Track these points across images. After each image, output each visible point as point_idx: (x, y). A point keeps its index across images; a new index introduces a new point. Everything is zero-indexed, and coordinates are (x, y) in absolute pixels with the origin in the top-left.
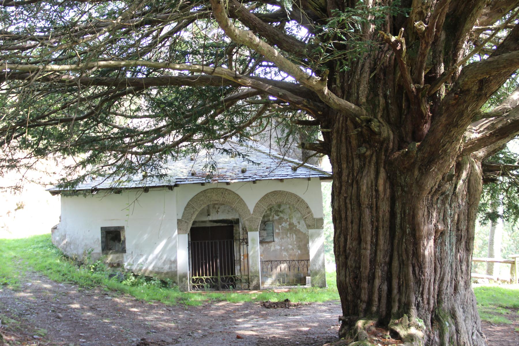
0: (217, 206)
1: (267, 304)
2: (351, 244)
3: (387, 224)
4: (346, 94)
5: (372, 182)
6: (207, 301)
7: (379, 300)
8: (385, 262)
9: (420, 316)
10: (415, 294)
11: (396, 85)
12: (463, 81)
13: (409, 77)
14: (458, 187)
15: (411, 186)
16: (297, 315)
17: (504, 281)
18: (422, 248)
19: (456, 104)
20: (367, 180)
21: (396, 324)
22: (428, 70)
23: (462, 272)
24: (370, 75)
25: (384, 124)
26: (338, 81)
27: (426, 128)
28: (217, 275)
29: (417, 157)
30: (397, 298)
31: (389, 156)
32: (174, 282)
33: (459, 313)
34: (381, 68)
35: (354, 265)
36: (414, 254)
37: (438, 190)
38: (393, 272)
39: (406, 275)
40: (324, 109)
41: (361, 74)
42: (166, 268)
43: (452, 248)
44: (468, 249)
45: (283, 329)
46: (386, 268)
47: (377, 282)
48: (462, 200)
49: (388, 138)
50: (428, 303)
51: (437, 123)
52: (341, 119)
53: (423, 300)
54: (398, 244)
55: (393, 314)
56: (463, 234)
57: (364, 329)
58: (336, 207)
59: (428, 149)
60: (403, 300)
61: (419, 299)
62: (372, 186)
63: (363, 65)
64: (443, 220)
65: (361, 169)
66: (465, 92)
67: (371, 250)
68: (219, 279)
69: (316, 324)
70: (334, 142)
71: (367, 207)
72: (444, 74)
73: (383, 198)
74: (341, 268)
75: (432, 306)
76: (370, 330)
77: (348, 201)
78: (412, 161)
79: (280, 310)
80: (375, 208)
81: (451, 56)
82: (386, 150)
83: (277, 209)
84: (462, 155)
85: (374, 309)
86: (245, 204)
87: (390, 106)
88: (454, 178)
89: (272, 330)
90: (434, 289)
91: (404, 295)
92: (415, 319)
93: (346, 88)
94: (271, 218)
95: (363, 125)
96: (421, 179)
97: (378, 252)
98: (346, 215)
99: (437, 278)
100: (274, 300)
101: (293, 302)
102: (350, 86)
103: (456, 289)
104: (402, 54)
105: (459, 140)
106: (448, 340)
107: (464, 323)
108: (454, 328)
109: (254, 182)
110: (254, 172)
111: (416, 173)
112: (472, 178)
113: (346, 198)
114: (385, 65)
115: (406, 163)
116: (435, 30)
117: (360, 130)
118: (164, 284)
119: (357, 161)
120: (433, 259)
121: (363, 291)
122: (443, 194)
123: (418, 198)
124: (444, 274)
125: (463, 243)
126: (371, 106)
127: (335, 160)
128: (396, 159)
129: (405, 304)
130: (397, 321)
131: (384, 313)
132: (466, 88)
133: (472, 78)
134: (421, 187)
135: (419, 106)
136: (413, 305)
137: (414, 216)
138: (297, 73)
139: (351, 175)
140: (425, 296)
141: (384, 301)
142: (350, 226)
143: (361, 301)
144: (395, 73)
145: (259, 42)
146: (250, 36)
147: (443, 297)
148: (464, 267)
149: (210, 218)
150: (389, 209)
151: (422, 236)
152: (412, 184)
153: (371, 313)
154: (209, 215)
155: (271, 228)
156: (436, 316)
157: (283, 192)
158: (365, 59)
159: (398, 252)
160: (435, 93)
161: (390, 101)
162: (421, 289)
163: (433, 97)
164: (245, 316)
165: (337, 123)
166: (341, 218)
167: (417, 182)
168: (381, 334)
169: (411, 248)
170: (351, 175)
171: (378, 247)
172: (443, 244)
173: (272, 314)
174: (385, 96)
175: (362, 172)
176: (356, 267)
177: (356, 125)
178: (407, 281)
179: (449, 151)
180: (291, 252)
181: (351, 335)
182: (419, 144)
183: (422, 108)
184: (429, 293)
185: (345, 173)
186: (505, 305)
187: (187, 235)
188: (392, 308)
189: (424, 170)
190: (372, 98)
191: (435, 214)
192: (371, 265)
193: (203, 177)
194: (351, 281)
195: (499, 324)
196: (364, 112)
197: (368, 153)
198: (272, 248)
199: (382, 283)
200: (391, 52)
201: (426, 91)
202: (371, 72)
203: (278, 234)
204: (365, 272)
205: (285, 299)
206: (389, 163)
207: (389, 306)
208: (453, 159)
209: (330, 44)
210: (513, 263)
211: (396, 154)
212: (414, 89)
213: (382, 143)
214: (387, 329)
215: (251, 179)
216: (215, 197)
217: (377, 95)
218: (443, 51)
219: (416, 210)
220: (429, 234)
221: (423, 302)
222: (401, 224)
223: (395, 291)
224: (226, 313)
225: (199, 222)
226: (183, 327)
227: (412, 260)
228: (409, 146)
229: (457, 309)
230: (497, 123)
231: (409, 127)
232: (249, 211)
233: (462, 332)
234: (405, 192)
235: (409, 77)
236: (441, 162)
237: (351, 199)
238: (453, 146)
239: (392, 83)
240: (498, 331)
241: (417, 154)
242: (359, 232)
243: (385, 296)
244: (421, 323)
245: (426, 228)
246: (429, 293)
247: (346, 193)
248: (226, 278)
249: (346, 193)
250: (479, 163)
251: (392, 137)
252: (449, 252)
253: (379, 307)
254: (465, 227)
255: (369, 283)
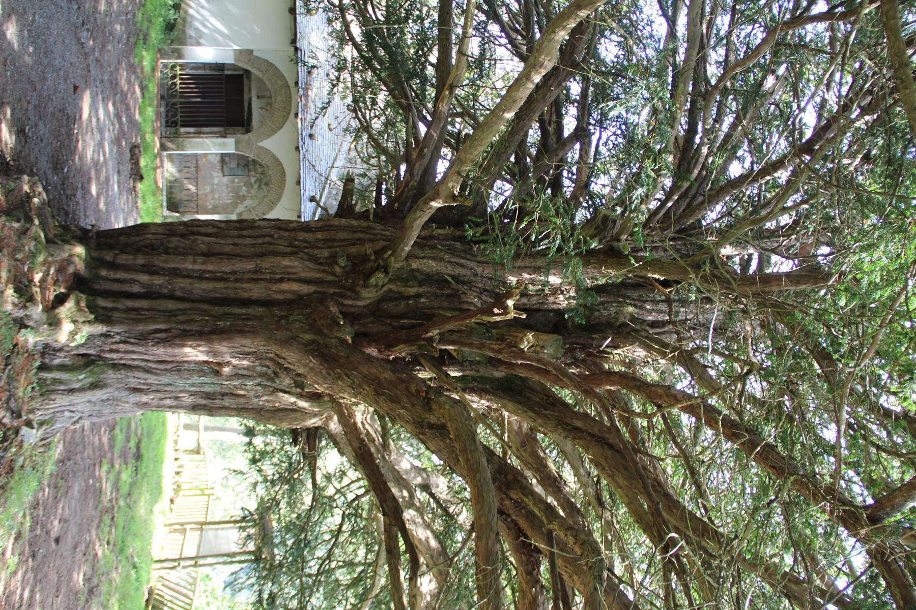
0: (268, 108)
1: (137, 151)
2: (202, 243)
3: (231, 294)
4: (423, 242)
5: (294, 274)
6: (142, 72)
7: (117, 280)
8: (174, 290)
9: (91, 337)
10: (125, 332)
11: (434, 311)
12: (445, 403)
13: (449, 326)
14: (286, 396)
15: (287, 329)
16: (119, 187)
17: (176, 442)
18: (194, 343)
19: (409, 392)
20: (297, 267)
21: (78, 303)
22: (455, 354)
23: (161, 399)
24: (449, 275)
25: (380, 293)
26: (440, 231)
27: (373, 351)
28: (181, 97)
29: (331, 338)
30: (119, 306)
31: (332, 299)
32: (172, 41)
33: (99, 394)
34: (458, 291)
35: (171, 245)
36: (185, 331)
37: (281, 368)
38: (159, 302)
39: (153, 320)
40: (402, 211)
41: (450, 262)
42: (191, 32)
43: (197, 386)
44: (195, 408)
45: (93, 159)
46: (165, 291)
47: (144, 278)
48: (267, 401)
49: (359, 298)
50: (111, 351)
51: (382, 366)
52: (388, 234)
53: (116, 343)
54: (200, 310)
55: (94, 300)
56: (216, 401)
57: (71, 256)
58: (259, 223)
59: (343, 354)
60: (116, 315)
61: (118, 338)
62: (289, 274)
63: (463, 266)
64: (237, 375)
65: (315, 260)
66: (427, 405)
67: (192, 270)
68: (175, 100)
69: (102, 206)
70: (354, 223)
71: (257, 266)
72: (448, 375)
73: (270, 289)
74: (168, 228)
75: (108, 355)
76: (68, 264)
77: (267, 239)
78: (326, 331)
79: (127, 166)
80: (256, 277)
81: (471, 385)
82: (341, 295)
83: (264, 181)
84: (333, 400)
85: (104, 273)
86: (269, 136)
87: (403, 303)
88: (299, 390)
89: (92, 144)
90: (128, 359)
91: (123, 316)
92: (87, 330)
93: (430, 243)
94: (253, 173)
95: (381, 261)
96: (299, 343)
97: (189, 281)
98: (246, 237)
99: (150, 365)
100: (143, 163)
101: (140, 186)
102: (433, 247)
103: (136, 390)
104: (488, 316)
105: (356, 397)
106: (57, 377)
107: (86, 400)
108: (77, 386)
109: (297, 148)
110: (310, 149)
111: (307, 337)
112: (299, 414)
113: (272, 236)
114: (463, 296)
115: (323, 322)
116: (519, 362)
117: (373, 257)
118: (170, 27)
119: (326, 253)
120: (178, 359)
121: (131, 257)
122: (276, 374)
123: (270, 338)
124: (156, 374)
125: (203, 402)
126: (405, 276)
127: (327, 223)
128: (327, 308)
129: (109, 317)
130: (83, 304)
131: (97, 287)
132: (434, 406)
133: (450, 414)
134: (286, 342)
135: (405, 342)
136: (109, 329)
137: (242, 332)
138: (471, 153)
139: (305, 245)
140: (122, 347)
141: (116, 287)
142: (229, 242)
143: (116, 254)
144: (449, 309)
145: (532, 82)
146: (546, 63)
147: (122, 371)
148: (168, 402)
149: (254, 99)
150: (253, 298)
151: (212, 343)
152: (291, 331)
153: (97, 267)
154: (258, 97)
155: (240, 173)
156: (93, 362)
157: (284, 184)
158: (471, 269)
159: (189, 309)
160: (421, 365)
161: (411, 302)
162: (133, 340)
163: (416, 361)
164: (118, 117)
165: (382, 228)
166: (242, 229)
167: (293, 338)
168: (61, 279)
169: (195, 327)
170: (305, 245)
171: (196, 281)
172: (202, 373)
173: (120, 153)
174: (418, 296)
175: (309, 260)
176: (168, 248)
177: (379, 253)
178: (145, 321)
179: (340, 382)
180: (210, 197)
181: (61, 236)
182: (350, 341)
183: (402, 346)
184: (126, 352)
185: (309, 236)
186: (143, 445)
187: (232, 62)
188: (104, 298)
189: (311, 347)
190: (416, 278)
191: (245, 362)
192: (169, 269)
193: (306, 84)
194: (148, 241)
195: (112, 440)
196: (398, 265)
197: (338, 270)
198: (215, 174)
199: (142, 285)
200: (479, 304)
201: (428, 351)
202: (453, 277)
203: (233, 182)
204: (159, 261)
205: (145, 175)
206: (322, 298)
207: (106, 294)
208: (327, 388)
209: (514, 204)
210: (198, 453)
211: (334, 309)
212: (430, 334)
213: (352, 289)
214: (70, 289)
215: (301, 143)
216: (279, 99)
217: (421, 285)
218: (478, 374)
219: (252, 336)
220: (215, 354)
221: (112, 343)
222: (231, 314)
223: (130, 303)
224: (122, 91)
225: (250, 85)
226: (98, 21)
227: (176, 329)
228: (348, 326)
229: (105, 391)
230: (375, 445)
231: (374, 328)
232: (261, 141)
233: (71, 397)
234: (279, 321)
235: (449, 326)
236: (324, 371)
237: (270, 243)
238: (347, 389)
239: (437, 305)
240: (100, 440)
241: (336, 337)
242: (220, 254)
243: (124, 289)
244: (80, 339)
245: (225, 350)
246: (126, 352)
247: (279, 238)
248: (177, 109)
249: (279, 238)
250: (319, 423)
251: (361, 303)
252: (190, 382)
253: (107, 279)
254: (227, 404)
255: (143, 266)
